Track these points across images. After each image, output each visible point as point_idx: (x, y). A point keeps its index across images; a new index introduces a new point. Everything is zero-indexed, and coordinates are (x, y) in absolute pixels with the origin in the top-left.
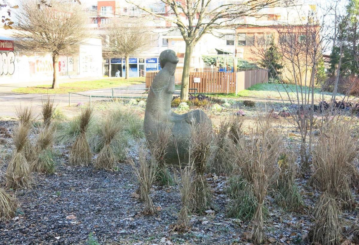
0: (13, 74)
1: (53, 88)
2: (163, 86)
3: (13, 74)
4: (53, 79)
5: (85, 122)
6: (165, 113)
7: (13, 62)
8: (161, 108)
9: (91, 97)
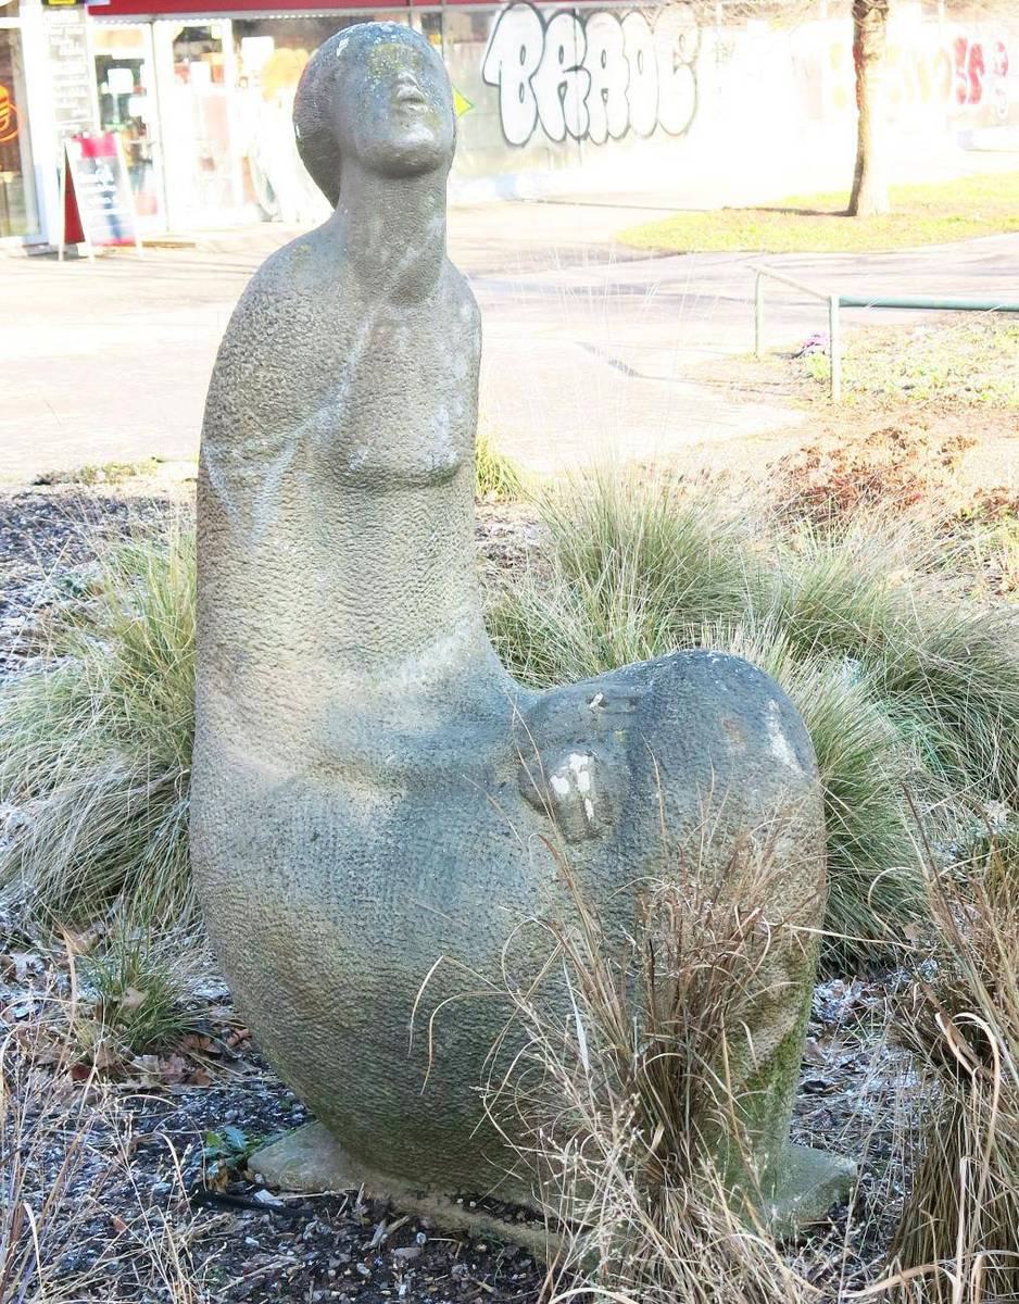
0: (686, 131)
1: (852, 211)
2: (296, 417)
3: (686, 131)
4: (854, 160)
5: (631, 540)
6: (346, 683)
7: (690, 65)
8: (288, 630)
9: (836, 303)
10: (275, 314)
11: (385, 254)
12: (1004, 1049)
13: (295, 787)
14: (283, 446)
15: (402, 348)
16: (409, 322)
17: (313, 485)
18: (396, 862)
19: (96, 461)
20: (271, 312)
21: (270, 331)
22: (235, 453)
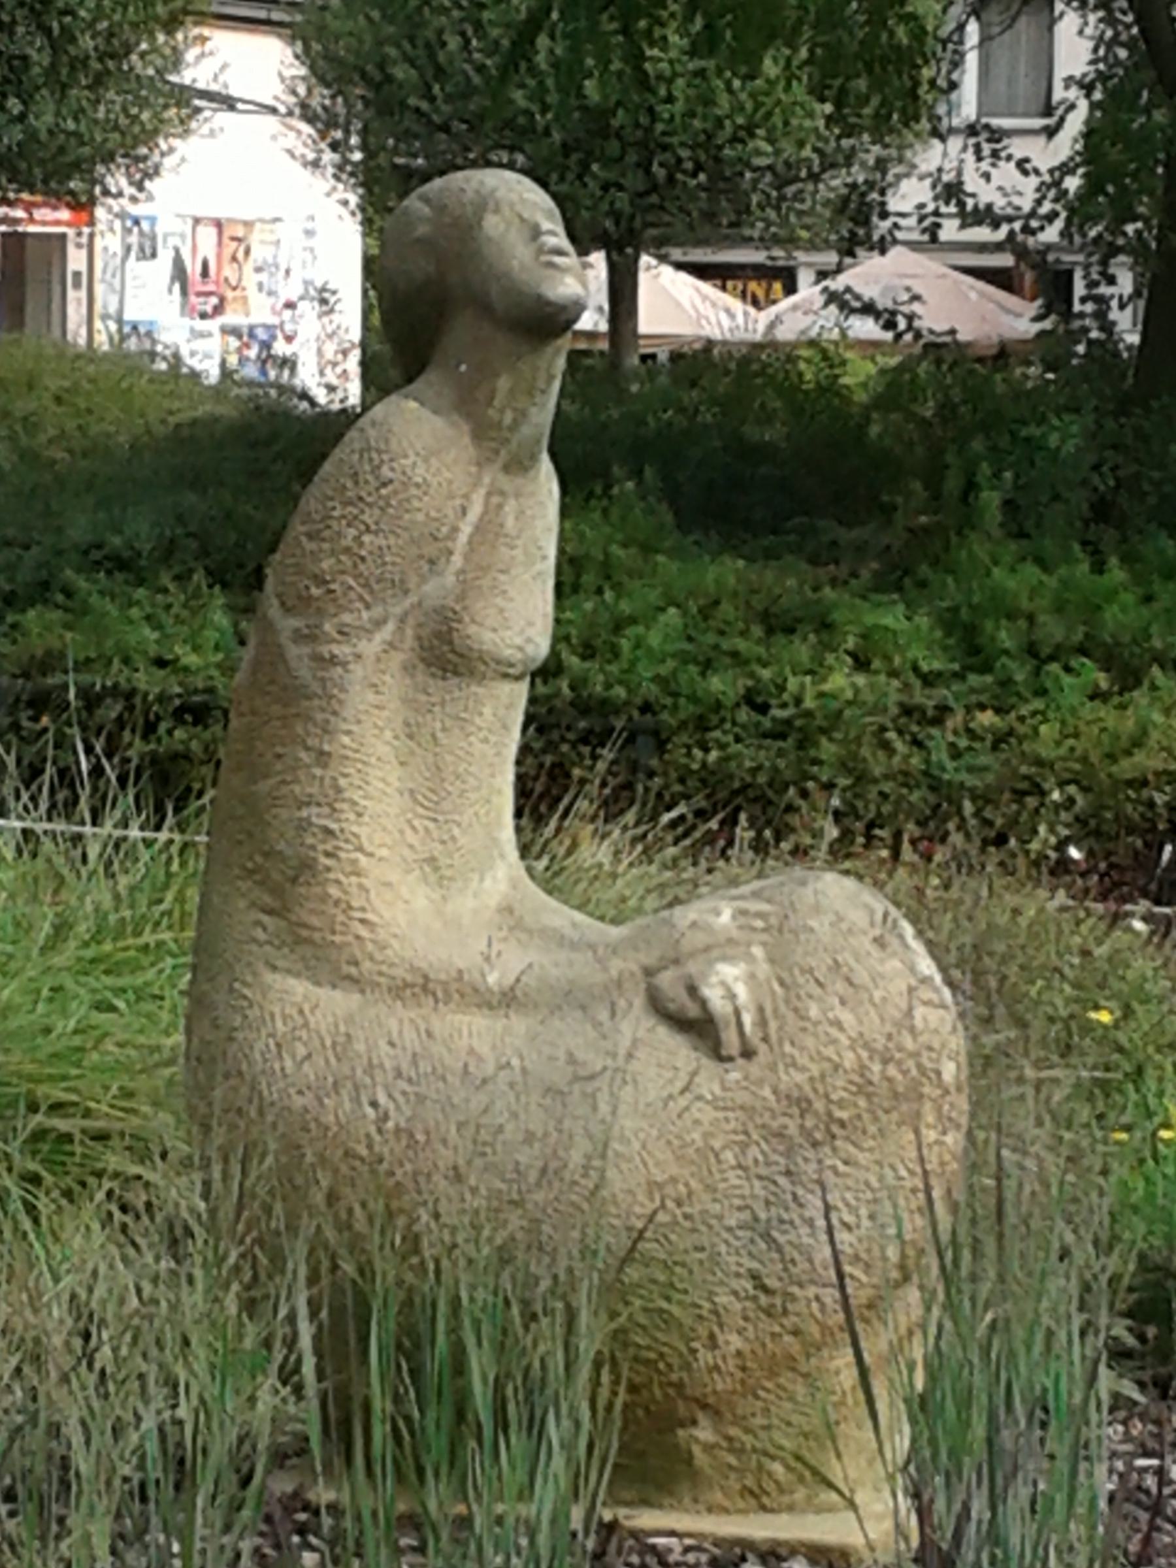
10: (390, 475)
11: (508, 418)
12: (1003, 1362)
13: (305, 933)
14: (384, 621)
15: (510, 522)
16: (518, 495)
17: (408, 669)
18: (129, 461)
19: (297, 166)
20: (385, 472)
21: (384, 491)
22: (327, 627)
